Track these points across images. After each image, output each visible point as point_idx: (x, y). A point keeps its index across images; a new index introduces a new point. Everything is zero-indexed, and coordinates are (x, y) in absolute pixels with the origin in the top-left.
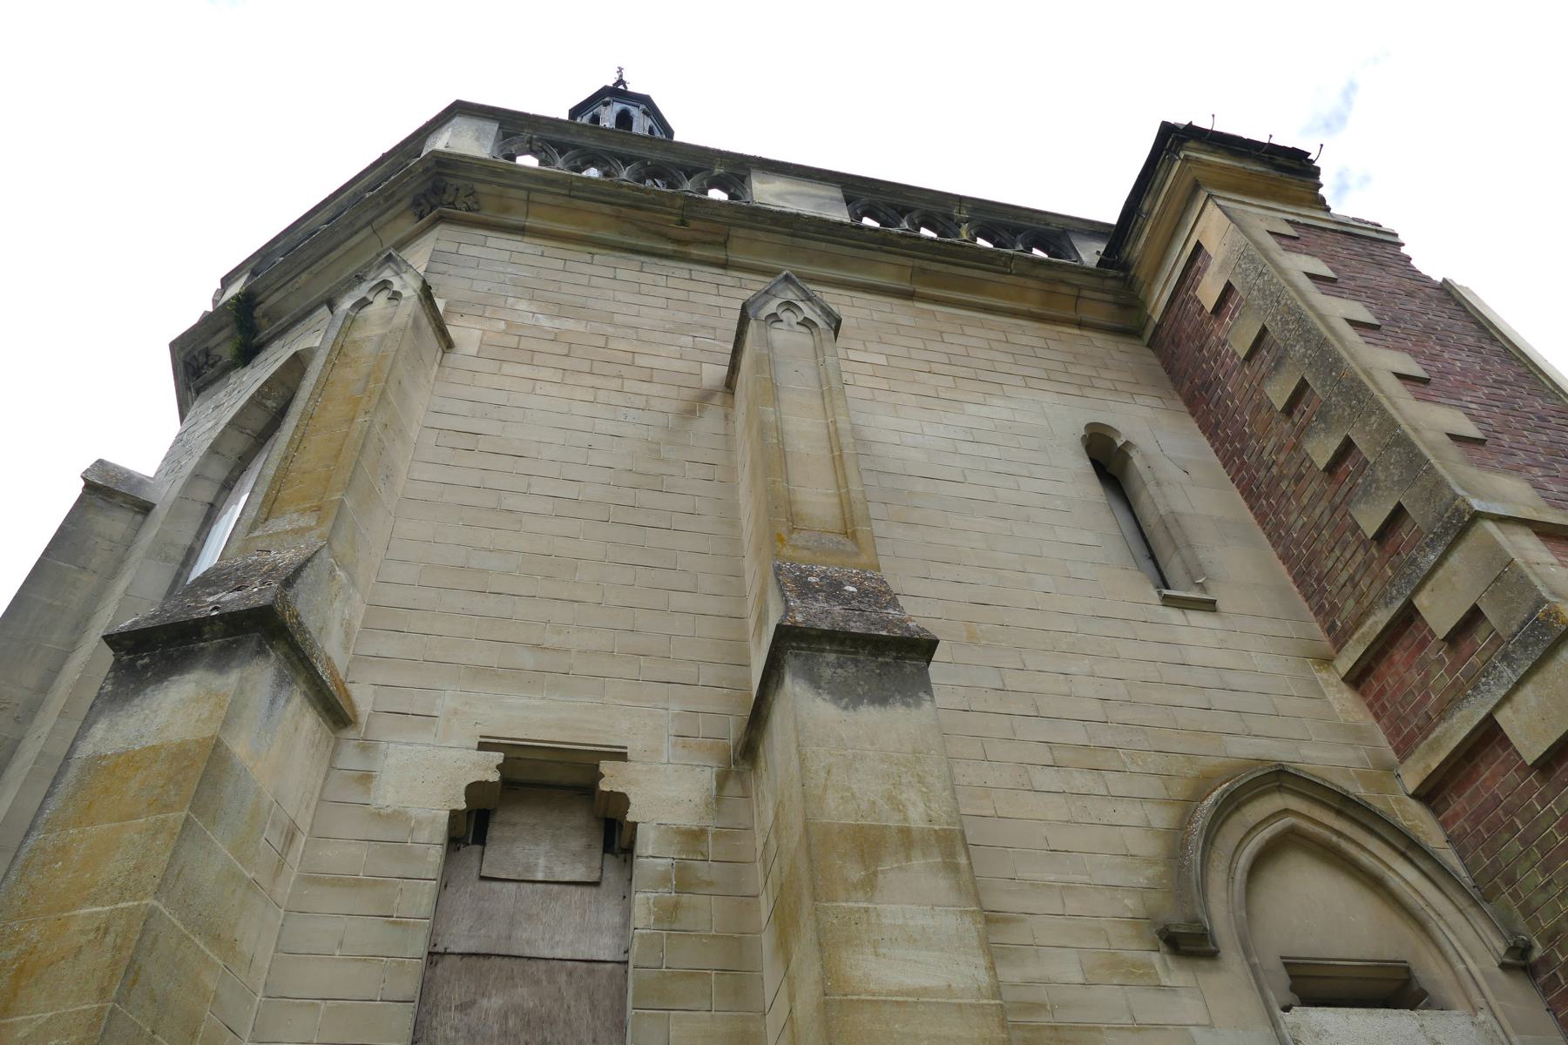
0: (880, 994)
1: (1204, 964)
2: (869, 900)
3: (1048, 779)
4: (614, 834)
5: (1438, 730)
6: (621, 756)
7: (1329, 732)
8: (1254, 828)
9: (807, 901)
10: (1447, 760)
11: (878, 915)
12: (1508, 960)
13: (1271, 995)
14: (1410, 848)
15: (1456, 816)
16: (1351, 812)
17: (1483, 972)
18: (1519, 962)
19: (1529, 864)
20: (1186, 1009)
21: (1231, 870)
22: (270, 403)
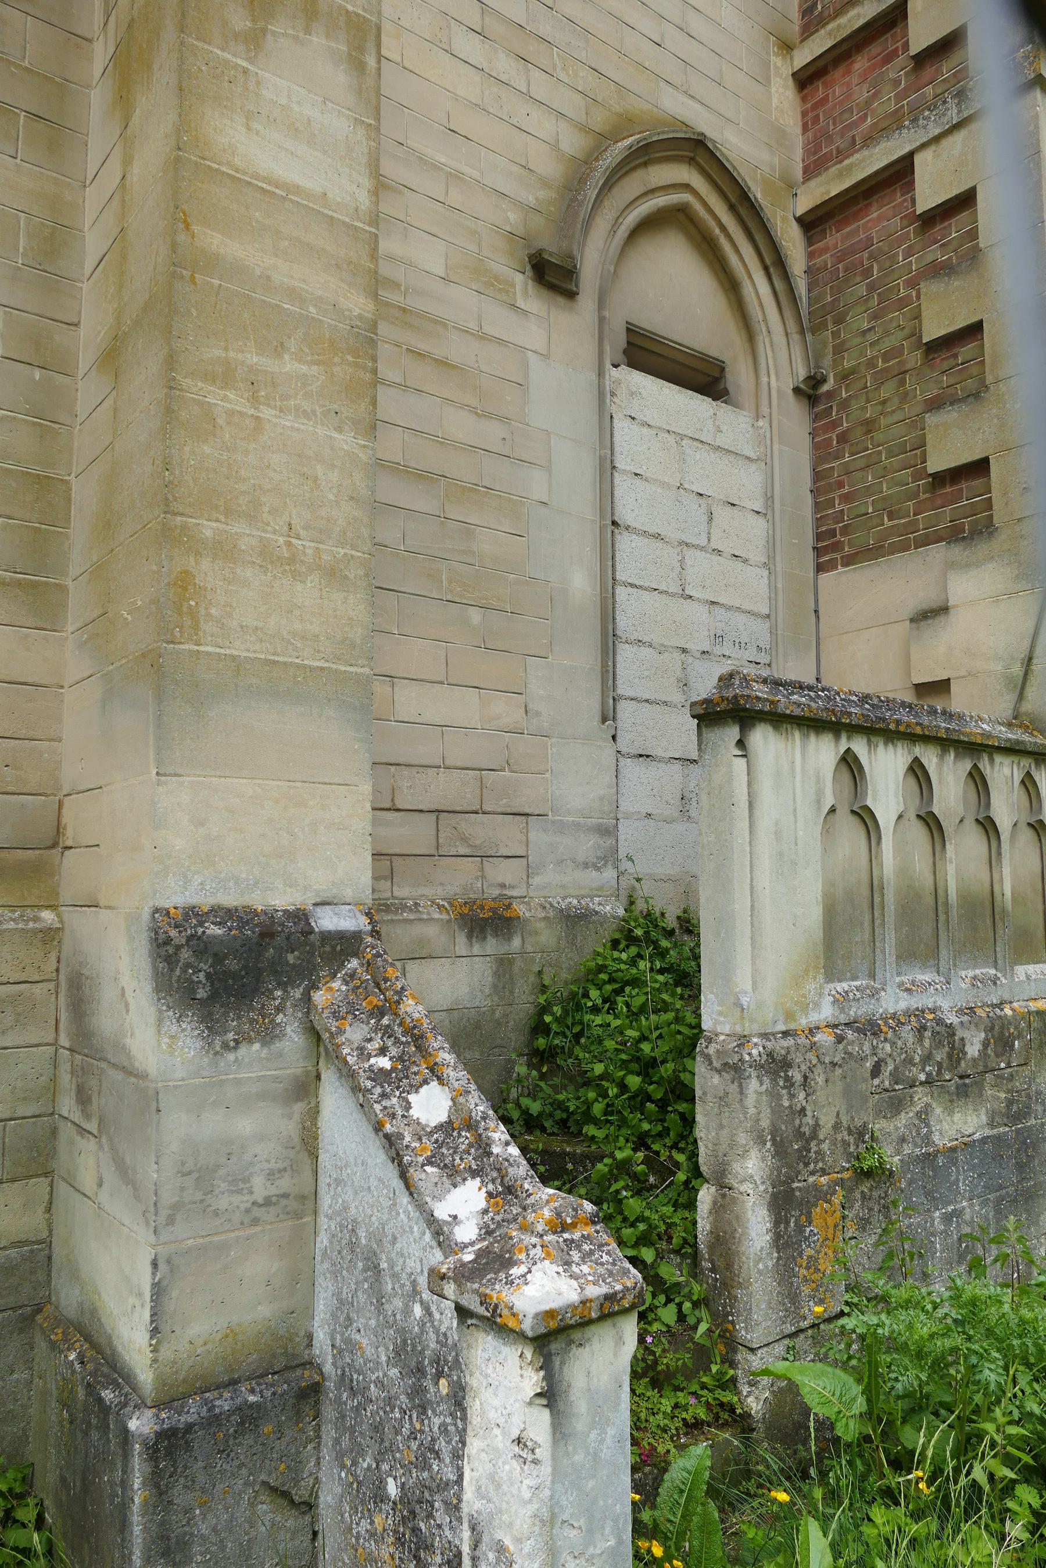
0: (245, 173)
1: (561, 300)
2: (249, 60)
5: (857, 156)
7: (755, 122)
8: (653, 191)
9: (169, 35)
10: (847, 190)
11: (258, 83)
12: (802, 386)
13: (607, 348)
14: (775, 263)
15: (826, 250)
16: (742, 211)
17: (779, 391)
18: (810, 392)
19: (864, 308)
20: (531, 335)
21: (616, 223)
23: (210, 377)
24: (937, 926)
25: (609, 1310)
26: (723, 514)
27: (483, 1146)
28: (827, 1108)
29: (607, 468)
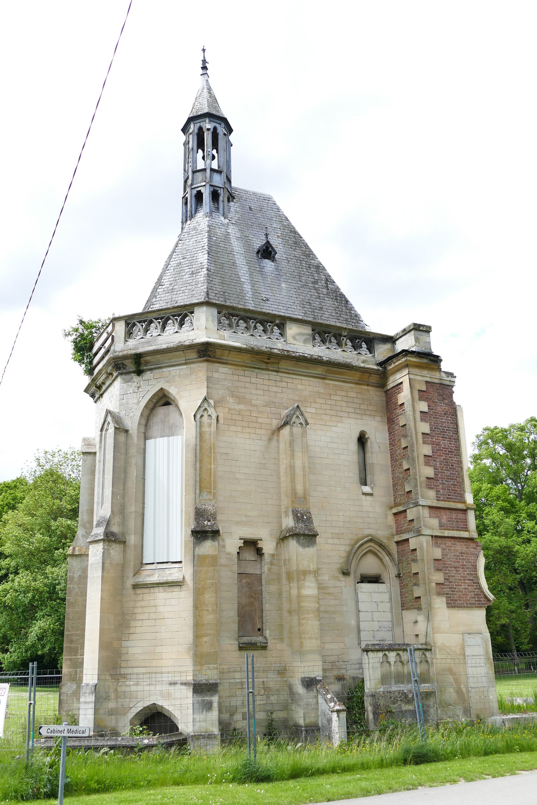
3: (330, 541)
4: (259, 552)
6: (261, 540)
20: (343, 584)
21: (357, 558)
22: (154, 400)
23: (303, 619)
24: (400, 678)
25: (343, 710)
26: (380, 605)
27: (334, 700)
28: (382, 702)
29: (357, 602)
